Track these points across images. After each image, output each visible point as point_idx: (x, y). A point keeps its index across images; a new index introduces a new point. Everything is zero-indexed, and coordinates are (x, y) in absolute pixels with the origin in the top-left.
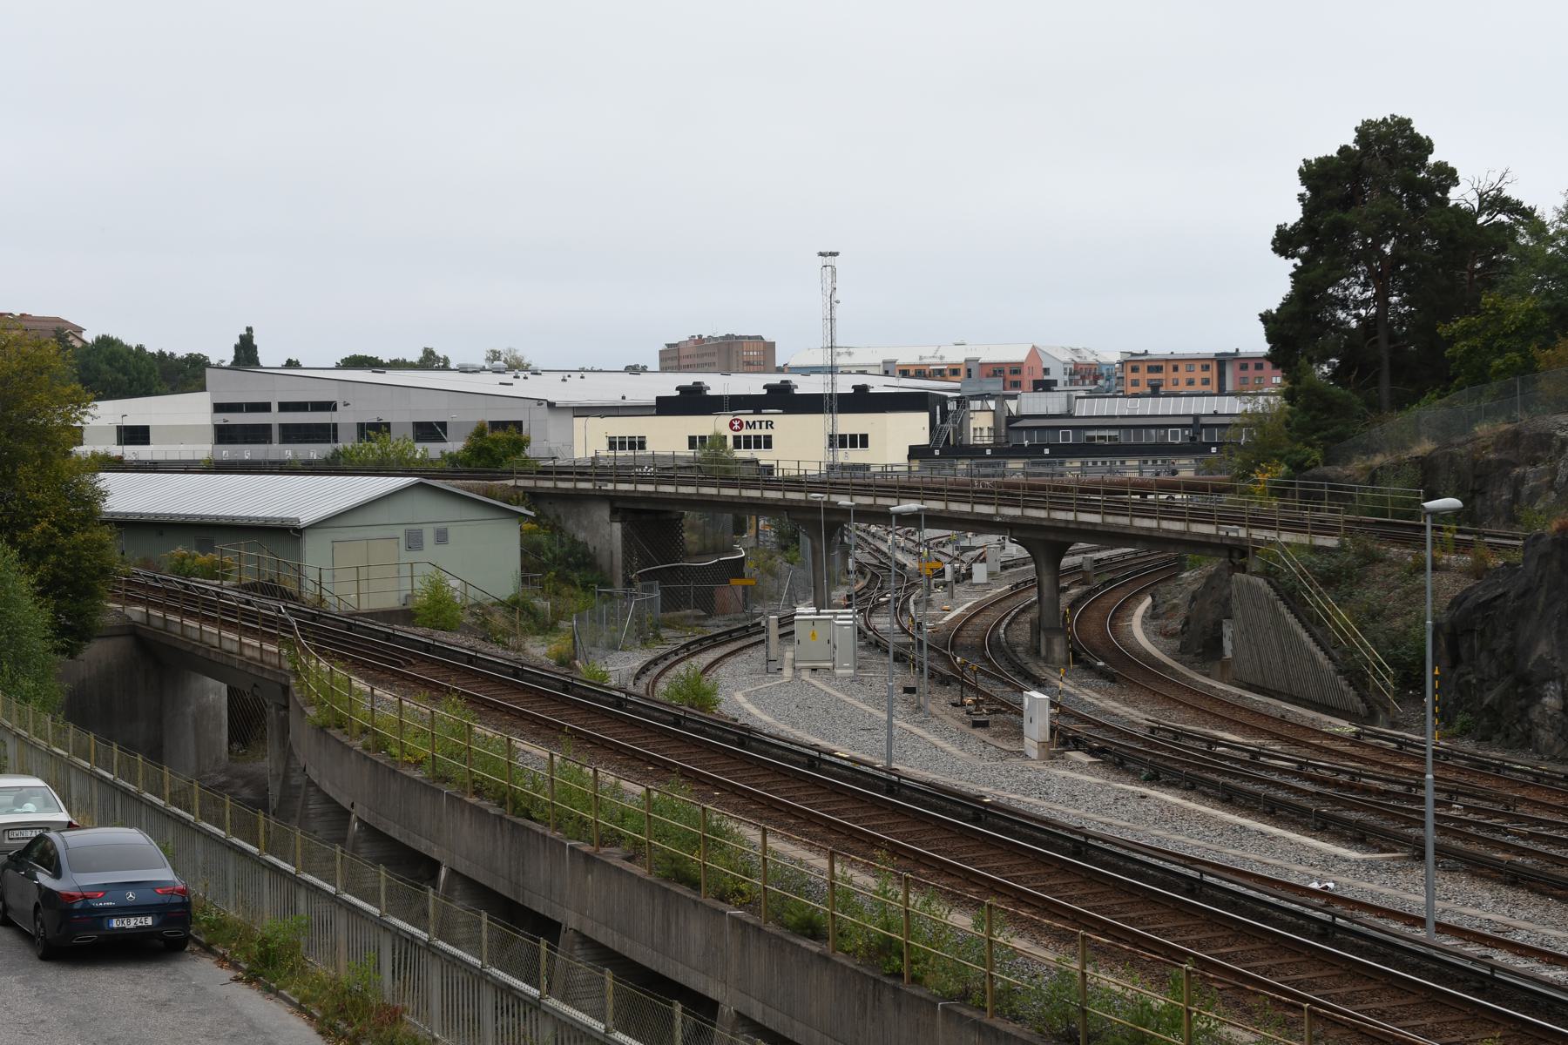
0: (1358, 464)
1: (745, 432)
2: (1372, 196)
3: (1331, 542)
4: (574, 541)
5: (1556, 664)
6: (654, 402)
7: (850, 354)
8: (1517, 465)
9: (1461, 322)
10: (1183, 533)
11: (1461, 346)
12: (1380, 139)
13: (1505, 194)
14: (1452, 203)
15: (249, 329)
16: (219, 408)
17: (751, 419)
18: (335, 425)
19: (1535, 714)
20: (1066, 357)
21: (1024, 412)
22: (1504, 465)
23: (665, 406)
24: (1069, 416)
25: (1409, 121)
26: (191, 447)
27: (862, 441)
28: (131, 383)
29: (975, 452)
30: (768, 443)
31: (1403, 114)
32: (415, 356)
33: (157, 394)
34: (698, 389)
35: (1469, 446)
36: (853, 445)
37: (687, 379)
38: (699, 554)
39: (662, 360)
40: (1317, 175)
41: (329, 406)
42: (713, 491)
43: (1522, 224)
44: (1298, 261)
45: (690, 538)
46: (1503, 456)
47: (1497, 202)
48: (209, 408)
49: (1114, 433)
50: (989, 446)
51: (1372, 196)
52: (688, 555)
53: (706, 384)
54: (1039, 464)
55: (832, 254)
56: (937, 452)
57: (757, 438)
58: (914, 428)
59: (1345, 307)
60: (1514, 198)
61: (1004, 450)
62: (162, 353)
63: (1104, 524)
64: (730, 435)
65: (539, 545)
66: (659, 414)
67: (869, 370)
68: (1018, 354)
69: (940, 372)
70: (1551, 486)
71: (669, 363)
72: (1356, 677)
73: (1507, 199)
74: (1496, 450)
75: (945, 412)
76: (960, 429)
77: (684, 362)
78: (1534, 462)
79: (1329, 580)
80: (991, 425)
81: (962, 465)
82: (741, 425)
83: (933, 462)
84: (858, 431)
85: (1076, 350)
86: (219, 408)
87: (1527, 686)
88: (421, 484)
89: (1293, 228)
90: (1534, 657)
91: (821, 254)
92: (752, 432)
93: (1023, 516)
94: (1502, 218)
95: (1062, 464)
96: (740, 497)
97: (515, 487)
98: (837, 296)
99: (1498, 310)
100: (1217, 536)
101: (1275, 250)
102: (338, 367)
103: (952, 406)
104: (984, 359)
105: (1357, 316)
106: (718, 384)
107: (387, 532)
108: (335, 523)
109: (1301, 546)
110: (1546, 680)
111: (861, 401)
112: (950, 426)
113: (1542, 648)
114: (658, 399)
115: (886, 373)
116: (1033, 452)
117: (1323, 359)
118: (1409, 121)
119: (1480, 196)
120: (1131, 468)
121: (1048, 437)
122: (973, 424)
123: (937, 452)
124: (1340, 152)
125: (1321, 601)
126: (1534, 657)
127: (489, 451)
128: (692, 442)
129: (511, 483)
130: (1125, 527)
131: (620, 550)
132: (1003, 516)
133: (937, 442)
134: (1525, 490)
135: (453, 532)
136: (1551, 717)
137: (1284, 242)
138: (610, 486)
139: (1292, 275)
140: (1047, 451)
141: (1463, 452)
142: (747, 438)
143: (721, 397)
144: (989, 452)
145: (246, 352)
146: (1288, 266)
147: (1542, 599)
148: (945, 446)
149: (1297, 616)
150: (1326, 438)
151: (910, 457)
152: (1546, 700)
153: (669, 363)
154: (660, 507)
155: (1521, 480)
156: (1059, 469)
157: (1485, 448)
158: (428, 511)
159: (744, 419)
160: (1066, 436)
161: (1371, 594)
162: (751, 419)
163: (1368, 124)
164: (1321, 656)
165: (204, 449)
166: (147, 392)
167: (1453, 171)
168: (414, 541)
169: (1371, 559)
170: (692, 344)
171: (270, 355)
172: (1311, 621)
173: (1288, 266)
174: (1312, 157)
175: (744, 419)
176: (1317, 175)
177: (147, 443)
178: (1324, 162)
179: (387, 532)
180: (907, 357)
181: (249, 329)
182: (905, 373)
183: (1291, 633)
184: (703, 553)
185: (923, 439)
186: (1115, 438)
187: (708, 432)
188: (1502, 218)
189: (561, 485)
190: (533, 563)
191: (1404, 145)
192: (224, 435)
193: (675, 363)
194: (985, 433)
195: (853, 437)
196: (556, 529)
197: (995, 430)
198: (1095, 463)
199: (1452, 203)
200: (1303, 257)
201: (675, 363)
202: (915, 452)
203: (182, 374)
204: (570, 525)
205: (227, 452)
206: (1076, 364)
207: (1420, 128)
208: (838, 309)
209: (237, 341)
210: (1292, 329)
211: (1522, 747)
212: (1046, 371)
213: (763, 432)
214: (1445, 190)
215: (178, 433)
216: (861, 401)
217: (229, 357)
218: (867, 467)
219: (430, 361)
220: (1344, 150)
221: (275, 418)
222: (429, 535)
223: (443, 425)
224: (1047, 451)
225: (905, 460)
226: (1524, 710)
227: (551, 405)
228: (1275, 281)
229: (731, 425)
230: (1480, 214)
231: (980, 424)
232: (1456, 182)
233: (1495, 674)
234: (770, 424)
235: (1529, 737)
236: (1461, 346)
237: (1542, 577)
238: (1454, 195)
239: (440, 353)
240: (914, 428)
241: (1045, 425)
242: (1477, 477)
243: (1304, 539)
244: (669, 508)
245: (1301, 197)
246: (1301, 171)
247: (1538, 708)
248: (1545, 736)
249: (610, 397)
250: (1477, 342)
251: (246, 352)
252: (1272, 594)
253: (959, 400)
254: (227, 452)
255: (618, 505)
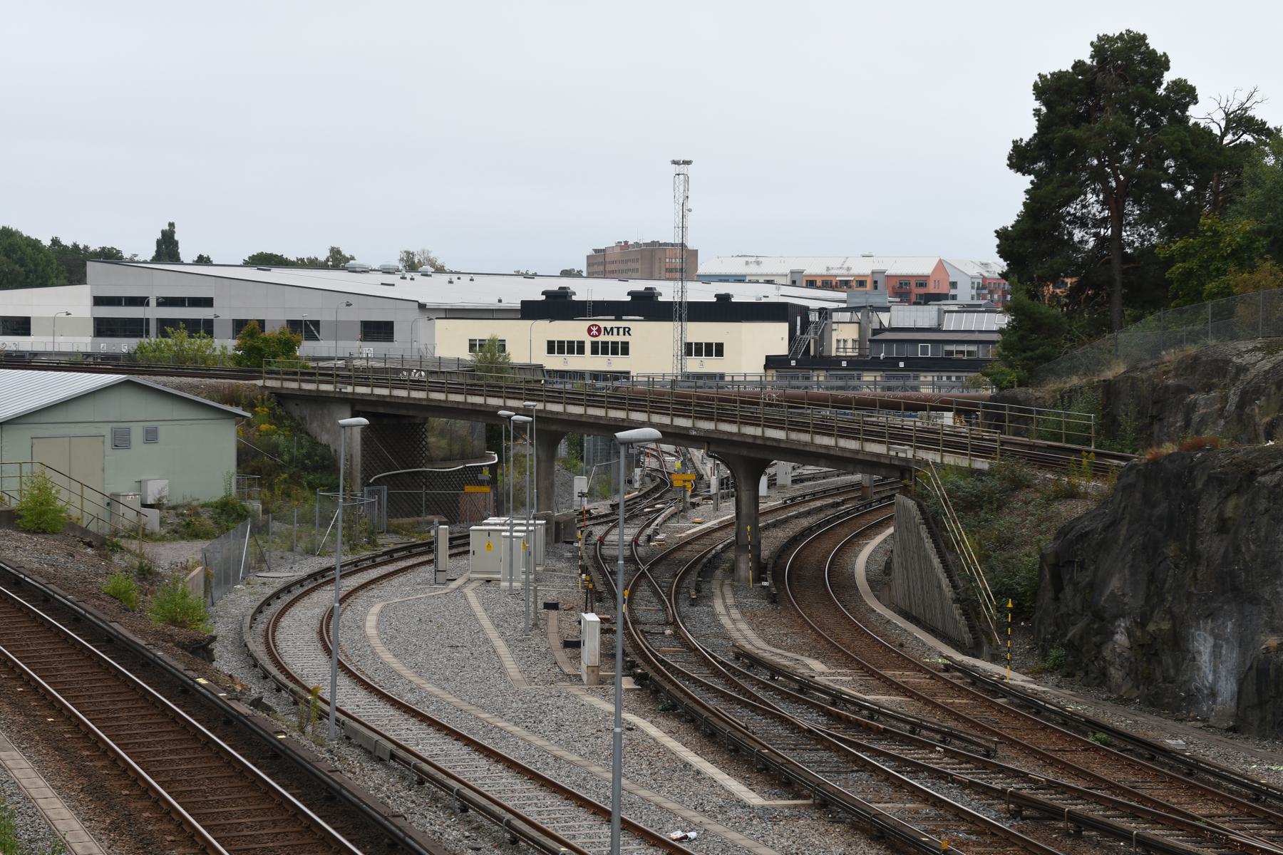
0: (1051, 387)
1: (602, 338)
2: (1106, 113)
3: (982, 464)
4: (315, 443)
5: (1126, 600)
6: (518, 306)
7: (758, 263)
8: (1191, 392)
9: (1180, 244)
10: (857, 452)
11: (1178, 267)
12: (1117, 54)
13: (1250, 113)
14: (1192, 122)
15: (172, 225)
16: (99, 301)
17: (609, 325)
18: (148, 320)
19: (1107, 653)
20: (974, 271)
21: (894, 325)
22: (1182, 390)
23: (529, 311)
24: (938, 330)
25: (1144, 37)
26: (70, 339)
27: (719, 350)
28: (28, 273)
29: (830, 363)
30: (625, 349)
31: (1138, 29)
32: (323, 255)
33: (53, 285)
34: (650, 295)
35: (1151, 371)
36: (709, 354)
37: (640, 286)
38: (444, 460)
39: (589, 265)
40: (1052, 91)
41: (208, 302)
42: (385, 392)
43: (1266, 144)
44: (1032, 177)
45: (435, 442)
46: (1181, 381)
47: (1240, 121)
48: (89, 301)
49: (973, 348)
50: (845, 358)
51: (1106, 113)
52: (431, 461)
53: (659, 290)
54: (894, 377)
55: (688, 163)
56: (793, 363)
57: (615, 344)
58: (775, 338)
59: (1083, 225)
60: (1258, 118)
61: (860, 364)
62: (76, 246)
63: (788, 440)
64: (588, 341)
65: (276, 446)
66: (523, 318)
67: (776, 280)
68: (924, 267)
69: (846, 283)
70: (1221, 413)
71: (596, 268)
72: (970, 607)
73: (1252, 119)
74: (1176, 376)
75: (806, 323)
76: (821, 340)
77: (610, 267)
78: (1208, 388)
79: (969, 505)
80: (856, 337)
81: (820, 376)
82: (599, 330)
83: (790, 373)
84: (714, 340)
85: (986, 265)
86: (99, 301)
87: (1102, 623)
88: (128, 382)
89: (1028, 144)
90: (1107, 592)
91: (675, 162)
92: (615, 338)
93: (717, 431)
94: (1247, 138)
95: (916, 378)
96: (465, 403)
97: (264, 387)
98: (689, 205)
99: (1216, 233)
100: (887, 456)
101: (1011, 166)
102: (247, 264)
103: (814, 317)
104: (892, 271)
105: (1096, 235)
106: (667, 291)
107: (90, 430)
108: (44, 418)
109: (958, 469)
110: (1117, 617)
111: (724, 310)
112: (811, 336)
113: (1115, 584)
114: (523, 302)
115: (794, 283)
116: (887, 365)
117: (1055, 279)
118: (1144, 37)
119: (1227, 114)
120: (925, 383)
121: (908, 351)
122: (835, 336)
123: (793, 363)
124: (1074, 67)
125: (955, 528)
126: (1107, 592)
127: (260, 350)
128: (472, 346)
129: (260, 383)
130: (806, 444)
131: (359, 448)
132: (698, 429)
133: (796, 353)
134: (1196, 418)
135: (163, 430)
136: (1120, 655)
137: (1020, 158)
138: (349, 389)
139: (1027, 192)
140: (902, 365)
141: (1144, 376)
142: (605, 344)
143: (584, 303)
144: (844, 364)
145: (167, 248)
146: (1026, 181)
147: (1124, 531)
148: (805, 357)
149: (935, 541)
150: (1032, 359)
151: (766, 367)
152: (1117, 637)
153: (596, 268)
154: (404, 412)
155: (1193, 407)
156: (911, 383)
157: (1166, 373)
158: (136, 409)
159: (602, 324)
160: (924, 350)
161: (1003, 522)
162: (609, 325)
163: (1104, 39)
164: (945, 582)
165: (84, 342)
166: (43, 282)
167: (1192, 89)
168: (121, 440)
169: (1018, 484)
170: (618, 250)
171: (187, 252)
172: (944, 546)
173: (1026, 181)
174: (1047, 71)
175: (602, 324)
176: (1052, 91)
177: (29, 334)
178: (1059, 76)
179: (90, 430)
180: (815, 268)
181: (172, 225)
182: (811, 284)
183: (927, 559)
184: (449, 459)
185: (782, 349)
186: (969, 353)
187: (486, 336)
188: (1247, 138)
189: (306, 386)
190: (252, 463)
191: (1141, 62)
192: (103, 328)
193: (601, 268)
194: (850, 344)
195: (709, 345)
196: (299, 429)
197: (860, 342)
198: (949, 378)
199: (1192, 122)
200: (1038, 174)
201: (601, 268)
202: (772, 362)
203: (65, 265)
204: (314, 427)
205: (107, 345)
206: (984, 278)
207: (1156, 44)
208: (690, 217)
209: (159, 236)
210: (1028, 244)
211: (1099, 685)
212: (954, 285)
213: (621, 338)
214: (1185, 108)
215: (55, 325)
216: (724, 310)
217: (149, 251)
218: (626, 375)
219: (337, 261)
220: (1079, 65)
221: (153, 313)
222: (137, 434)
223: (316, 324)
224: (902, 365)
225: (762, 371)
226: (1099, 646)
227: (422, 307)
228: (1010, 195)
229: (590, 331)
230: (1224, 135)
231: (844, 337)
232: (1195, 100)
233: (1079, 607)
234: (627, 331)
235: (1104, 675)
236: (1178, 267)
237: (1125, 508)
238: (1196, 114)
239: (346, 253)
240: (775, 338)
241: (907, 337)
242: (1155, 403)
243: (963, 462)
244: (411, 413)
245: (1037, 112)
246: (1036, 87)
247: (1110, 645)
248: (1115, 674)
249: (489, 301)
250: (1193, 264)
251: (167, 248)
252: (918, 517)
253: (822, 311)
254: (107, 345)
255: (358, 408)
